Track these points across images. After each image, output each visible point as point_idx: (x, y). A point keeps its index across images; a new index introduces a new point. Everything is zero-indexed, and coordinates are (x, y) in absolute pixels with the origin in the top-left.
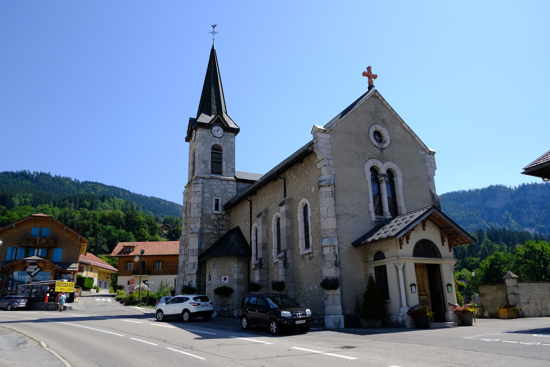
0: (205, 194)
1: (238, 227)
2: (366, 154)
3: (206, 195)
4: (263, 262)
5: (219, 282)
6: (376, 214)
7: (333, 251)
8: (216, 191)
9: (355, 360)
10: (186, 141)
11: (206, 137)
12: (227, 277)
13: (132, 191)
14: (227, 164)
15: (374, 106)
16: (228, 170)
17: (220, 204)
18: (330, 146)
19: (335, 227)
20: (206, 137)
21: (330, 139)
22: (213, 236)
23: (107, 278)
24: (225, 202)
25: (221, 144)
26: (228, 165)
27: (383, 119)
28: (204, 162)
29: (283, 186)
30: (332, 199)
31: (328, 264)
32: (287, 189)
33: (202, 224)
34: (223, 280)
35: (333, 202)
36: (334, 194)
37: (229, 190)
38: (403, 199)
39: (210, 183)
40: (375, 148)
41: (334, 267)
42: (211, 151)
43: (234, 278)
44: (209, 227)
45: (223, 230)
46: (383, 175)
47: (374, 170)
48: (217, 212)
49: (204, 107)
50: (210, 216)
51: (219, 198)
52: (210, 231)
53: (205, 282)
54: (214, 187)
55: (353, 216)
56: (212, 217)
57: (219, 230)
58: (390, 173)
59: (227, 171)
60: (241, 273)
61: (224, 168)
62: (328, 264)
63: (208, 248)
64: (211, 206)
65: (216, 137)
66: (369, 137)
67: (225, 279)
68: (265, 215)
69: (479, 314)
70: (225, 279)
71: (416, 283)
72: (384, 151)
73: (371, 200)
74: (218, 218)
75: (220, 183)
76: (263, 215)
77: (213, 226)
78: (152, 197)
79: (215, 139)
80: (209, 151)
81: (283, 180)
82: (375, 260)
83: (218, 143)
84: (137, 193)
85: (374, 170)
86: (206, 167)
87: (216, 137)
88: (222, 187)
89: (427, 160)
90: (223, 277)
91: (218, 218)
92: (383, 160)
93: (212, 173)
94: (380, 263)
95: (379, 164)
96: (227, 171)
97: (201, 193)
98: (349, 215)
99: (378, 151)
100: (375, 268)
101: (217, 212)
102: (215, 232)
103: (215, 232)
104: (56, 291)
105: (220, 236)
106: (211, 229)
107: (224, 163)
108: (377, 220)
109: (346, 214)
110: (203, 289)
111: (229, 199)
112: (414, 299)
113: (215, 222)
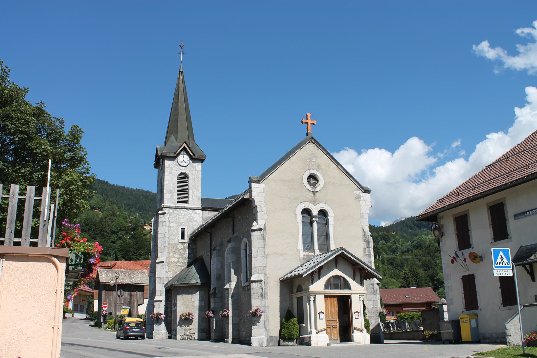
1: (202, 256)
4: (217, 292)
6: (304, 251)
8: (182, 220)
10: (155, 167)
13: (111, 182)
14: (193, 192)
16: (194, 198)
17: (186, 233)
20: (172, 166)
21: (263, 188)
23: (83, 300)
25: (187, 172)
27: (318, 164)
28: (170, 192)
30: (262, 241)
33: (169, 253)
35: (262, 244)
37: (195, 219)
40: (307, 192)
44: (176, 255)
46: (316, 217)
47: (306, 212)
49: (172, 129)
50: (176, 245)
53: (171, 308)
56: (178, 246)
58: (323, 213)
63: (174, 276)
69: (451, 337)
71: (324, 311)
72: (316, 194)
73: (301, 239)
75: (186, 212)
76: (218, 248)
77: (180, 255)
78: (138, 190)
80: (176, 180)
81: (209, 234)
82: (297, 292)
84: (119, 185)
85: (306, 212)
86: (172, 197)
89: (362, 198)
92: (315, 202)
93: (178, 202)
95: (311, 207)
97: (167, 224)
98: (278, 254)
100: (297, 298)
101: (183, 241)
106: (177, 258)
107: (190, 192)
109: (275, 253)
110: (170, 314)
112: (156, 327)
113: (182, 251)
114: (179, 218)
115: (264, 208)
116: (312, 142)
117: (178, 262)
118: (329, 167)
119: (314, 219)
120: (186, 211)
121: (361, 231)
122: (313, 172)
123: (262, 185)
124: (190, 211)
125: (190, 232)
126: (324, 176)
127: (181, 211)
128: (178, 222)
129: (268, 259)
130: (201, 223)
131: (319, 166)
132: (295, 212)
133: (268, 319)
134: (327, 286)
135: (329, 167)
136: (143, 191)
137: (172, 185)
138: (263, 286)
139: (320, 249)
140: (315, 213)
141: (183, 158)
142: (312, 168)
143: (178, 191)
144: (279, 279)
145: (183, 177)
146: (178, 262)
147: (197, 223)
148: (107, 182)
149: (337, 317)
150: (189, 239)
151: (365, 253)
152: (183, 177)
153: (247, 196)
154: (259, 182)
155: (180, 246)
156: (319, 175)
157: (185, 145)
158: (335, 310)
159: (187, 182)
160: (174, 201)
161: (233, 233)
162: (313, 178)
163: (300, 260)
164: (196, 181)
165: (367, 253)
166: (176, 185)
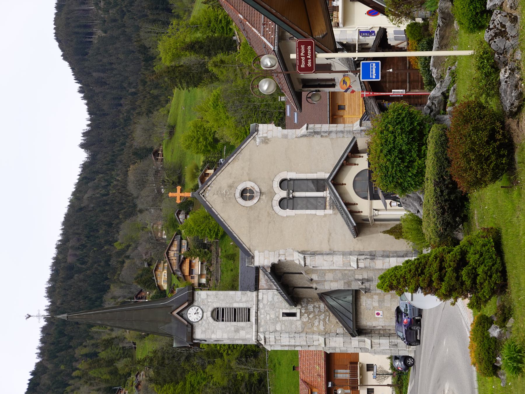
0: (278, 329)
2: (268, 212)
3: (278, 328)
5: (381, 320)
7: (362, 261)
8: (273, 316)
11: (204, 329)
12: (376, 312)
16: (244, 300)
18: (266, 252)
19: (342, 256)
20: (204, 329)
21: (259, 252)
22: (327, 319)
24: (285, 304)
25: (211, 309)
26: (238, 300)
28: (237, 331)
30: (317, 257)
31: (372, 264)
32: (294, 272)
33: (313, 333)
34: (379, 316)
35: (320, 256)
36: (314, 254)
37: (270, 299)
38: (309, 174)
39: (262, 323)
41: (374, 261)
43: (377, 305)
44: (316, 324)
45: (319, 307)
46: (288, 194)
48: (298, 315)
50: (304, 323)
51: (281, 311)
52: (321, 322)
54: (268, 317)
55: (330, 234)
56: (305, 320)
57: (320, 311)
58: (283, 183)
59: (246, 302)
60: (372, 298)
61: (241, 305)
62: (372, 264)
64: (291, 322)
65: (203, 316)
66: (251, 207)
67: (378, 314)
70: (378, 314)
72: (263, 190)
73: (313, 212)
74: (305, 313)
75: (262, 311)
77: (316, 319)
79: (205, 317)
80: (221, 324)
83: (209, 314)
85: (282, 203)
86: (243, 328)
87: (203, 316)
88: (267, 309)
89: (265, 135)
90: (376, 316)
91: (305, 313)
95: (277, 198)
96: (246, 302)
97: (277, 334)
99: (264, 197)
101: (298, 315)
102: (322, 317)
103: (322, 317)
105: (327, 311)
106: (319, 322)
107: (236, 305)
108: (332, 207)
109: (329, 241)
111: (281, 299)
113: (311, 316)
114: (270, 320)
115: (281, 252)
117: (324, 320)
118: (231, 174)
119: (291, 196)
120: (261, 311)
121: (302, 138)
122: (238, 194)
123: (256, 254)
124: (261, 306)
125: (287, 305)
126: (241, 181)
127: (261, 317)
128: (276, 321)
129: (335, 250)
130: (276, 292)
132: (284, 217)
133: (396, 252)
135: (231, 174)
136: (53, 279)
137: (228, 329)
138: (363, 257)
139: (324, 190)
140: (283, 194)
141: (192, 315)
142: (233, 194)
143: (235, 321)
144: (355, 238)
145: (218, 315)
146: (324, 320)
147: (276, 297)
148: (33, 373)
150: (296, 306)
151: (326, 136)
152: (218, 315)
153: (269, 270)
155: (305, 319)
156: (240, 188)
157: (175, 313)
159: (223, 309)
160: (249, 326)
161: (301, 273)
163: (335, 214)
164: (222, 297)
165: (327, 134)
166: (228, 323)
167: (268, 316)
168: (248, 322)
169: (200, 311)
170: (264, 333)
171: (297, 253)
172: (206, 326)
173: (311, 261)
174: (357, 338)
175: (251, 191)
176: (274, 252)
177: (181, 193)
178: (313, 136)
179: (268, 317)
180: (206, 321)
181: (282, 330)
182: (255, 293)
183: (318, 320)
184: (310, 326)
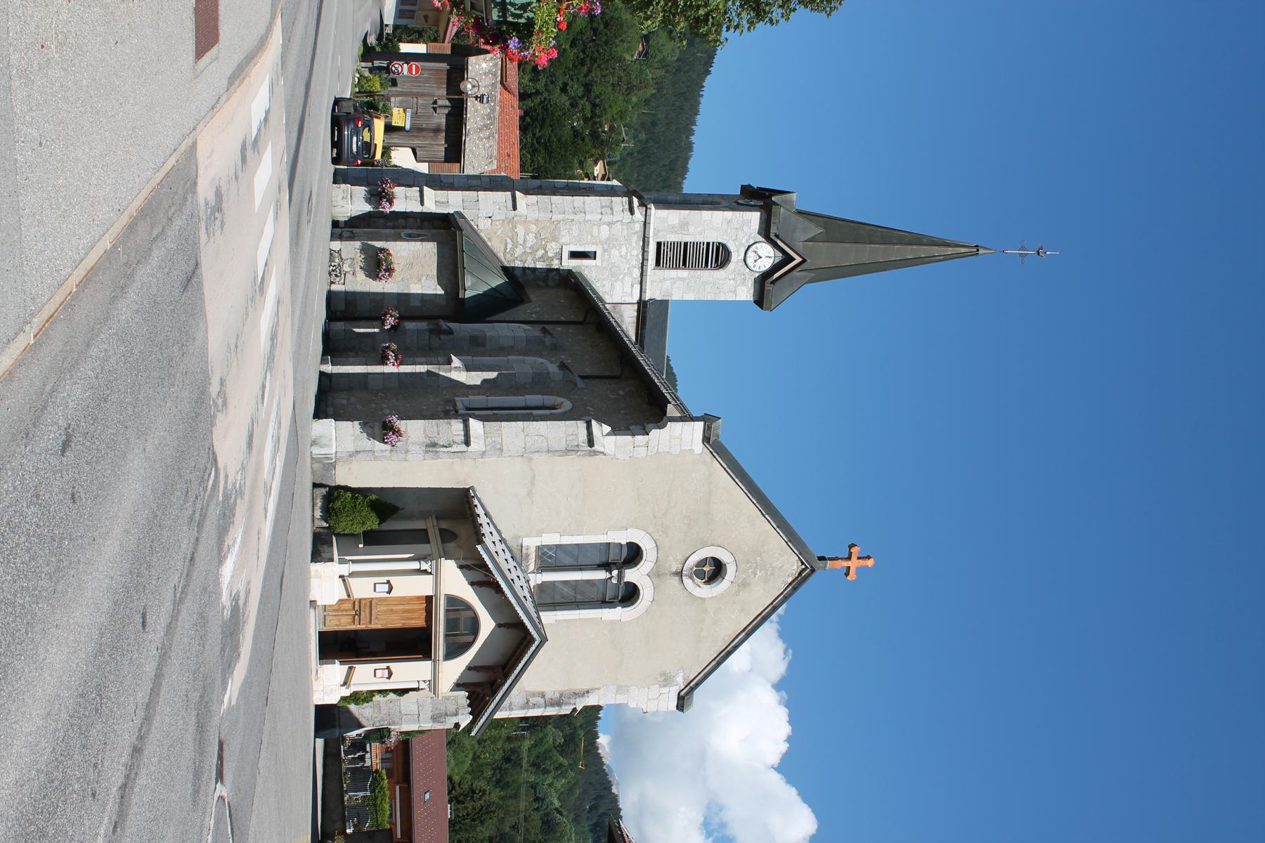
4: (443, 337)
8: (615, 252)
9: (217, 582)
10: (743, 187)
13: (709, 82)
15: (778, 564)
16: (668, 284)
20: (746, 229)
21: (691, 450)
23: (426, 17)
25: (731, 266)
26: (679, 283)
28: (684, 225)
29: (607, 374)
37: (618, 285)
40: (680, 557)
42: (711, 241)
44: (531, 239)
46: (620, 576)
47: (633, 554)
49: (837, 230)
50: (555, 239)
51: (598, 261)
54: (624, 250)
55: (529, 493)
56: (553, 244)
58: (630, 595)
63: (482, 235)
68: (548, 343)
71: (393, 594)
72: (677, 578)
75: (634, 262)
76: (548, 340)
77: (531, 247)
80: (713, 238)
81: (581, 319)
82: (441, 530)
85: (633, 554)
86: (672, 229)
89: (665, 690)
92: (656, 575)
93: (659, 244)
94: (434, 534)
95: (646, 566)
98: (532, 484)
99: (675, 567)
101: (565, 255)
102: (519, 251)
103: (519, 251)
104: (358, 244)
106: (525, 241)
107: (683, 273)
109: (534, 478)
111: (600, 291)
113: (541, 252)
114: (620, 246)
115: (642, 452)
116: (803, 570)
117: (515, 245)
119: (615, 572)
121: (585, 687)
123: (698, 447)
124: (637, 272)
125: (586, 273)
126: (720, 597)
127: (637, 252)
128: (610, 243)
129: (520, 459)
130: (607, 299)
131: (744, 585)
134: (452, 601)
136: (687, 159)
140: (631, 575)
141: (766, 257)
142: (740, 569)
143: (686, 244)
145: (719, 256)
147: (607, 288)
149: (379, 626)
150: (570, 271)
151: (533, 695)
152: (719, 256)
153: (671, 410)
154: (706, 439)
155: (552, 248)
158: (395, 622)
160: (660, 234)
161: (583, 377)
162: (714, 571)
163: (517, 537)
165: (533, 700)
166: (699, 239)
167: (623, 253)
168: (662, 240)
169: (750, 261)
170: (633, 222)
171: (606, 451)
172: (740, 234)
173: (577, 435)
174: (450, 210)
175: (699, 573)
176: (658, 452)
177: (849, 568)
178: (561, 695)
179: (624, 250)
180: (741, 244)
181: (599, 226)
182: (647, 297)
183: (528, 245)
184: (543, 232)
